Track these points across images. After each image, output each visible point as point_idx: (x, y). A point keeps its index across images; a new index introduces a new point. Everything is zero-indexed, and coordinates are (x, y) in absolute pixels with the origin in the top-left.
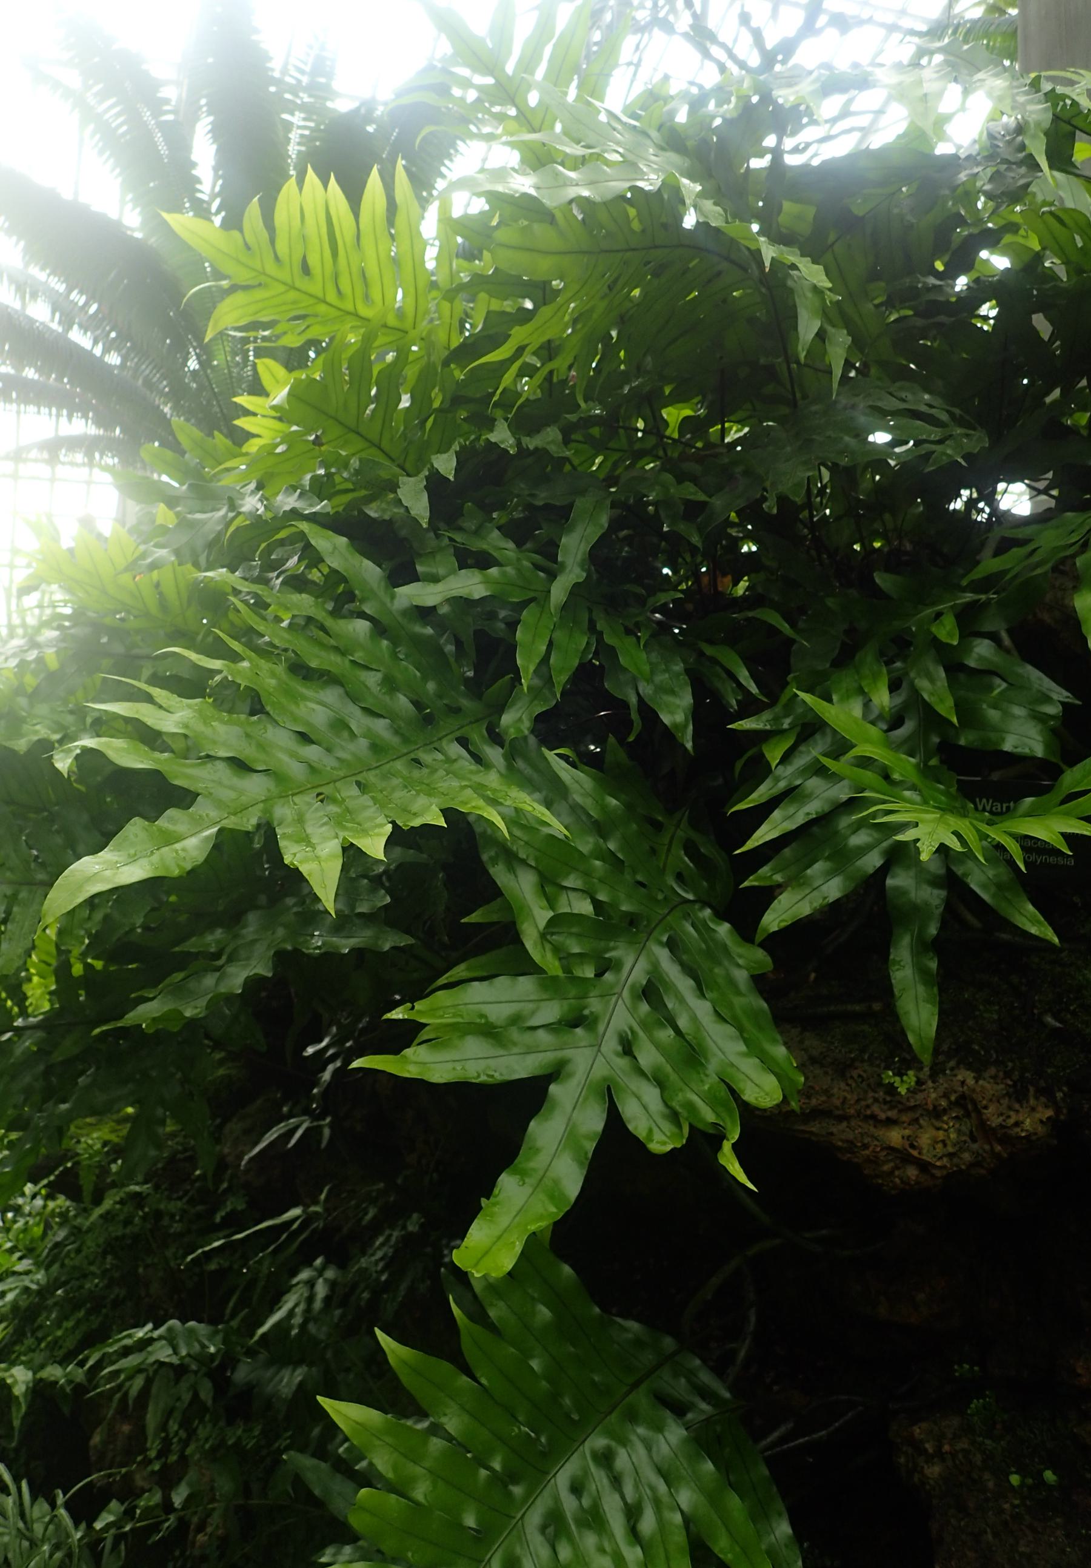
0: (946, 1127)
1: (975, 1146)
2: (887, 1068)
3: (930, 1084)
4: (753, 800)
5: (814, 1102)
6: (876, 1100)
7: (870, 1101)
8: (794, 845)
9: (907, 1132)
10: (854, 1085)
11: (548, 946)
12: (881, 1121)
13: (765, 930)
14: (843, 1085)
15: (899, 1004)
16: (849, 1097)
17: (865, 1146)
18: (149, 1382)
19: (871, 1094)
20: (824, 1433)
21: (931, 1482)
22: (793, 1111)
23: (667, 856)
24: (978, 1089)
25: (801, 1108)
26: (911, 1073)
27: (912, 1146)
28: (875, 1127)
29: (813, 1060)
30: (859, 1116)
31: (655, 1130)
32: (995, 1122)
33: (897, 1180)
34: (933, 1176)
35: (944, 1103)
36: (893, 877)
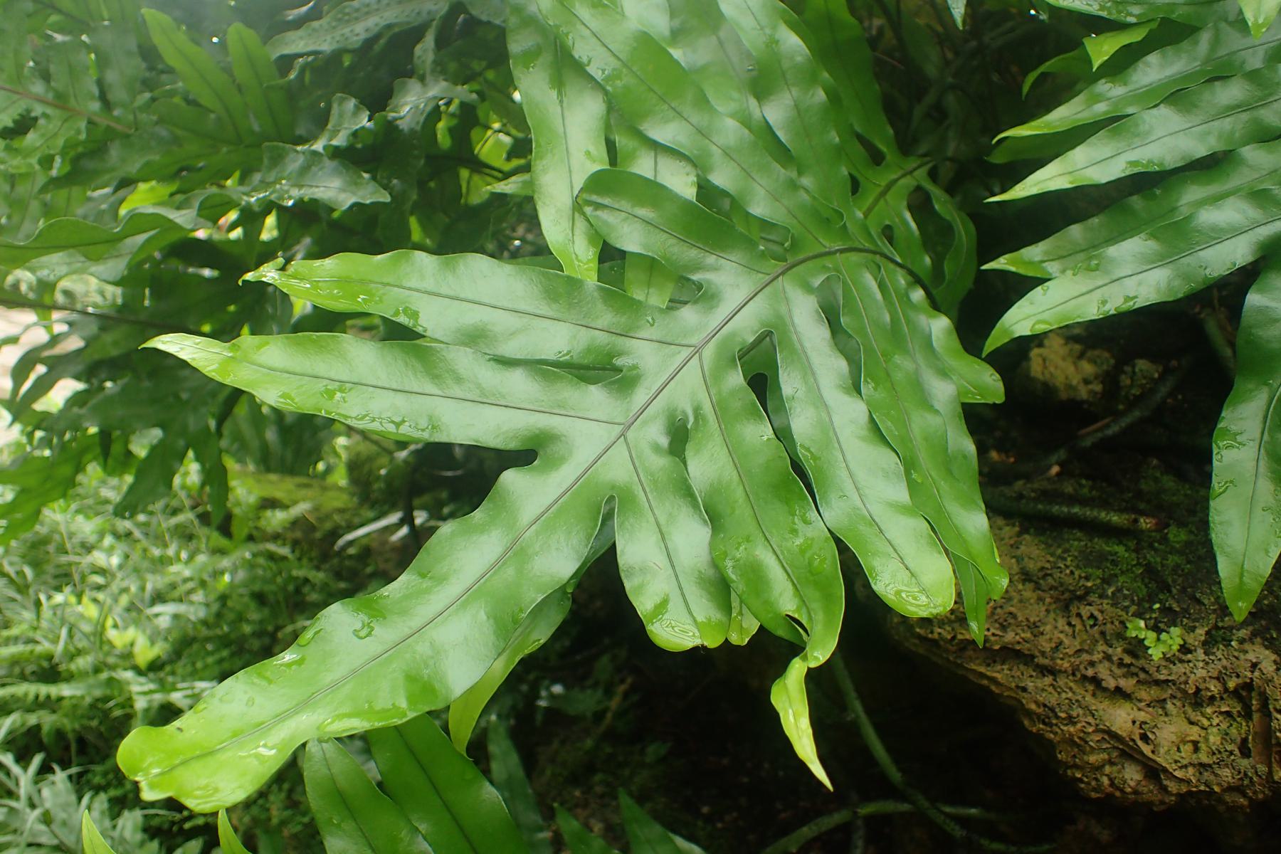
0: (1206, 723)
1: (1244, 763)
2: (1139, 615)
3: (1200, 654)
4: (1048, 125)
5: (1010, 637)
6: (1108, 657)
7: (1096, 657)
8: (1095, 221)
9: (1142, 716)
10: (1079, 627)
11: (581, 225)
12: (1105, 690)
13: (1006, 331)
14: (1061, 623)
15: (1213, 504)
16: (1066, 641)
17: (1071, 720)
19: (1101, 647)
22: (973, 642)
23: (876, 201)
25: (986, 641)
26: (1176, 631)
27: (1144, 738)
28: (1094, 695)
29: (1026, 576)
30: (1074, 674)
31: (675, 606)
33: (1105, 781)
34: (1164, 789)
35: (1214, 688)
36: (1260, 291)
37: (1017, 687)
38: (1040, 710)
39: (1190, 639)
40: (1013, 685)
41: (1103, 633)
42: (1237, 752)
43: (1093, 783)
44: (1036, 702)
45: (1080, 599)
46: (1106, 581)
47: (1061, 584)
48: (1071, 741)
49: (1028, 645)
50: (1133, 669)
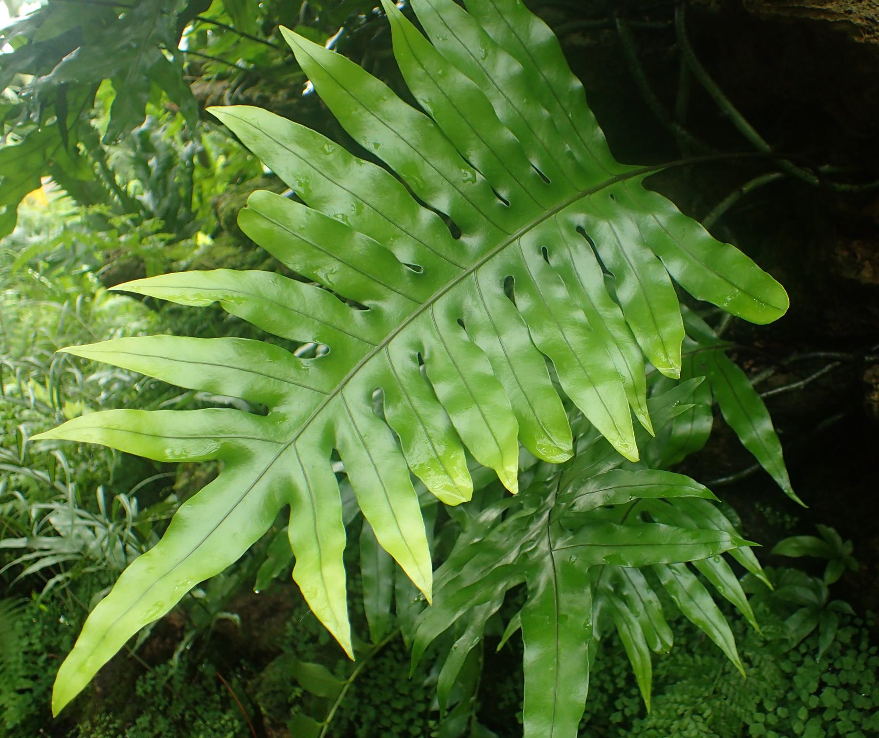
20: (801, 383)
37: (846, 12)
38: (865, 23)
40: (842, 11)
44: (861, 18)
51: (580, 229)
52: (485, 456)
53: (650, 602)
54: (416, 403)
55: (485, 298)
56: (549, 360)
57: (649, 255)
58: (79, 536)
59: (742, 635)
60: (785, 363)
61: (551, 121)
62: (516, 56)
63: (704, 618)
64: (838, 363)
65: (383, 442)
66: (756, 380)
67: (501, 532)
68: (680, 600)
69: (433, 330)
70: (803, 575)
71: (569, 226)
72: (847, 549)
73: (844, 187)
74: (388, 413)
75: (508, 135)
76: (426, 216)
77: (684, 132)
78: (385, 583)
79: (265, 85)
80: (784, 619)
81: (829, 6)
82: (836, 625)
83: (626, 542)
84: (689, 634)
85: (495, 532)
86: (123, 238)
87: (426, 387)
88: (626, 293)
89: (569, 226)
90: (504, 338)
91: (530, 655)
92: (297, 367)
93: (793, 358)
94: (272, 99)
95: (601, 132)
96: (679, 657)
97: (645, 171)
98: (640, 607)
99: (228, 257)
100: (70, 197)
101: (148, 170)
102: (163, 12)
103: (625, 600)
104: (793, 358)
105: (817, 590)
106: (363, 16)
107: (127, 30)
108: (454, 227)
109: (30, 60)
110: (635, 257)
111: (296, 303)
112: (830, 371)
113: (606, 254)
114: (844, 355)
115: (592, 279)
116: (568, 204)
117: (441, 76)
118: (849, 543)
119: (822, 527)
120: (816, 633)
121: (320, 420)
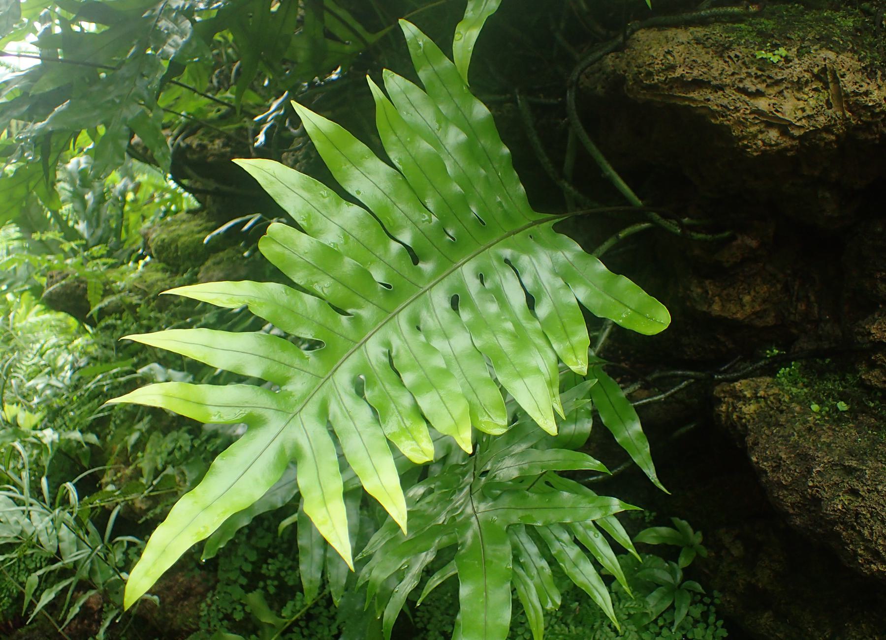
0: (806, 97)
3: (796, 60)
5: (695, 73)
6: (749, 75)
7: (743, 76)
9: (773, 101)
14: (721, 62)
16: (727, 68)
17: (737, 109)
18: (92, 562)
19: (744, 70)
20: (662, 396)
21: (747, 416)
24: (838, 61)
27: (777, 111)
32: (850, 88)
33: (760, 143)
35: (807, 76)
38: (720, 109)
39: (790, 54)
40: (702, 99)
41: (744, 63)
42: (825, 106)
43: (754, 147)
45: (728, 48)
46: (741, 37)
47: (717, 42)
48: (739, 122)
49: (706, 76)
50: (764, 78)
51: (507, 261)
52: (443, 426)
53: (543, 568)
54: (388, 387)
55: (437, 311)
56: (491, 358)
57: (560, 282)
58: (17, 522)
59: (618, 598)
60: (649, 379)
61: (487, 178)
62: (464, 130)
63: (586, 581)
64: (692, 381)
65: (364, 413)
66: (627, 391)
67: (428, 503)
68: (566, 567)
69: (399, 335)
70: (660, 561)
71: (499, 258)
72: (697, 538)
73: (700, 236)
74: (368, 394)
75: (457, 188)
76: (395, 247)
77: (571, 188)
78: (318, 553)
79: (203, 135)
80: (645, 596)
81: (691, 95)
82: (689, 601)
83: (536, 506)
84: (576, 595)
85: (423, 503)
86: (69, 261)
87: (395, 375)
88: (542, 310)
89: (499, 258)
90: (451, 341)
91: (464, 591)
92: (302, 357)
93: (656, 375)
94: (209, 147)
95: (522, 187)
96: (556, 627)
97: (554, 218)
98: (535, 572)
99: (157, 281)
100: (14, 225)
101: (84, 203)
102: (143, 75)
103: (522, 566)
104: (656, 375)
105: (672, 572)
106: (306, 84)
107: (111, 88)
108: (414, 256)
109: (25, 108)
110: (549, 283)
111: (300, 309)
112: (686, 386)
113: (527, 280)
114: (698, 374)
115: (517, 300)
116: (498, 242)
117: (409, 142)
118: (699, 533)
119: (676, 520)
120: (672, 607)
121: (317, 398)
